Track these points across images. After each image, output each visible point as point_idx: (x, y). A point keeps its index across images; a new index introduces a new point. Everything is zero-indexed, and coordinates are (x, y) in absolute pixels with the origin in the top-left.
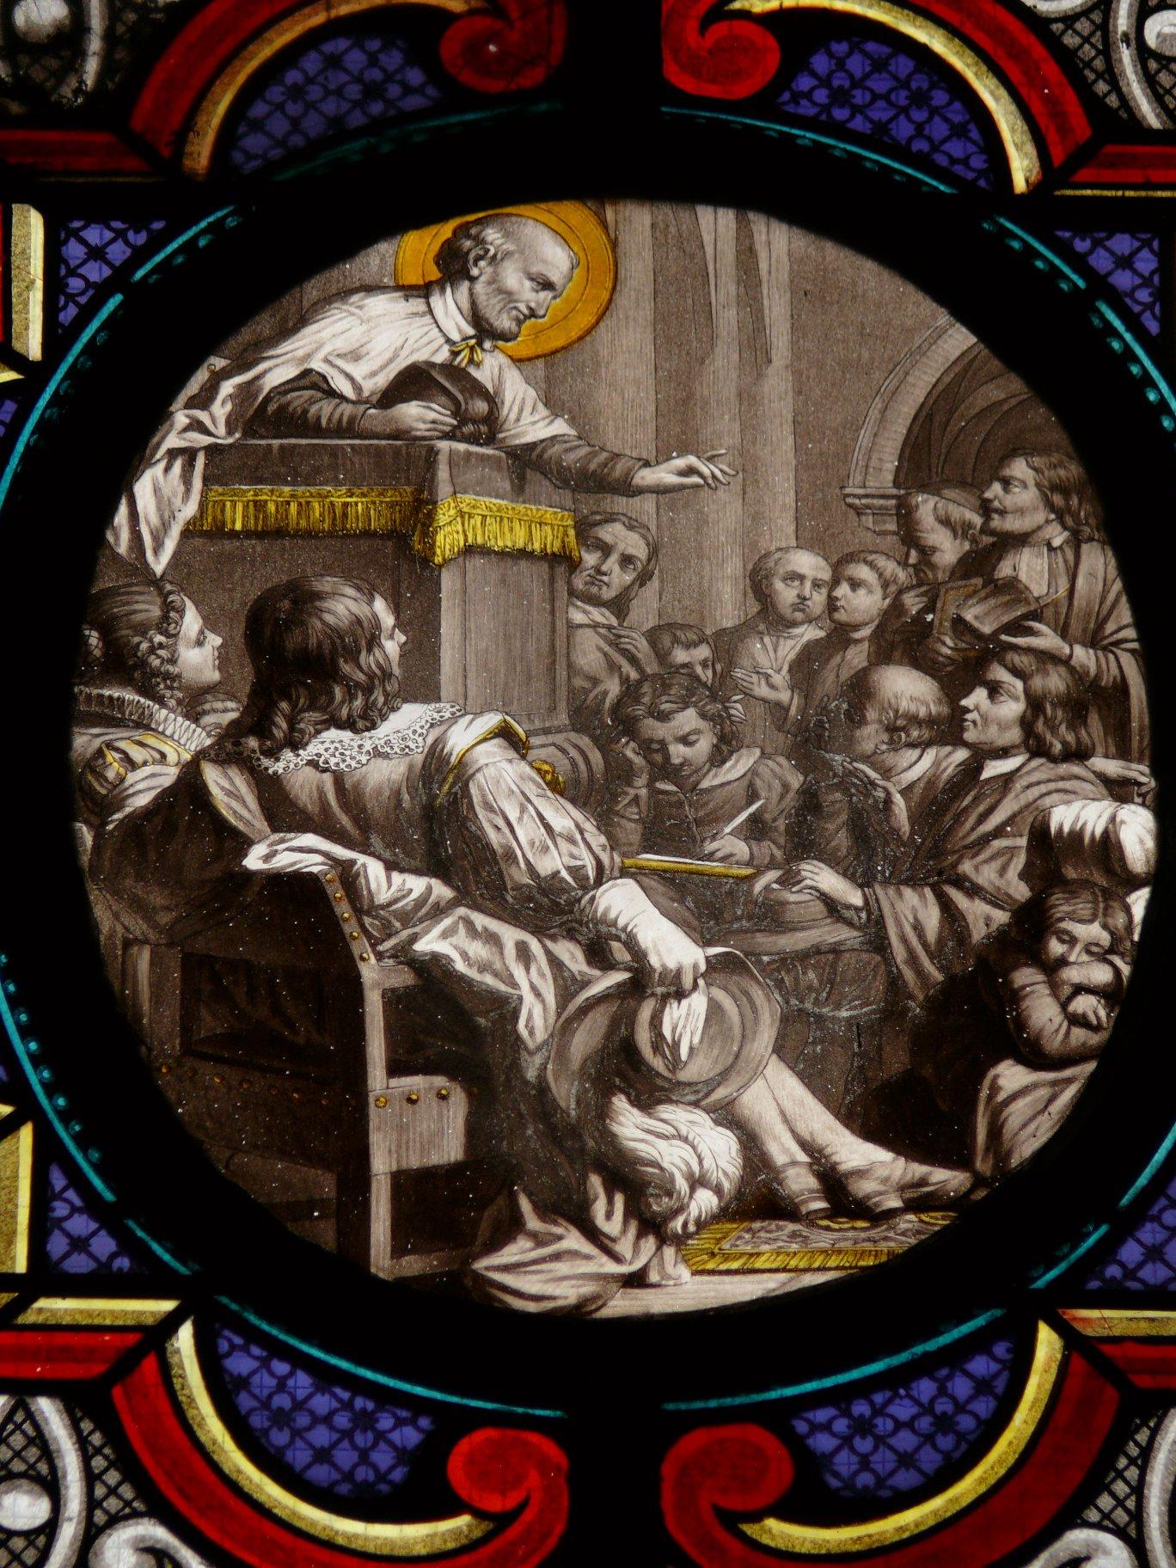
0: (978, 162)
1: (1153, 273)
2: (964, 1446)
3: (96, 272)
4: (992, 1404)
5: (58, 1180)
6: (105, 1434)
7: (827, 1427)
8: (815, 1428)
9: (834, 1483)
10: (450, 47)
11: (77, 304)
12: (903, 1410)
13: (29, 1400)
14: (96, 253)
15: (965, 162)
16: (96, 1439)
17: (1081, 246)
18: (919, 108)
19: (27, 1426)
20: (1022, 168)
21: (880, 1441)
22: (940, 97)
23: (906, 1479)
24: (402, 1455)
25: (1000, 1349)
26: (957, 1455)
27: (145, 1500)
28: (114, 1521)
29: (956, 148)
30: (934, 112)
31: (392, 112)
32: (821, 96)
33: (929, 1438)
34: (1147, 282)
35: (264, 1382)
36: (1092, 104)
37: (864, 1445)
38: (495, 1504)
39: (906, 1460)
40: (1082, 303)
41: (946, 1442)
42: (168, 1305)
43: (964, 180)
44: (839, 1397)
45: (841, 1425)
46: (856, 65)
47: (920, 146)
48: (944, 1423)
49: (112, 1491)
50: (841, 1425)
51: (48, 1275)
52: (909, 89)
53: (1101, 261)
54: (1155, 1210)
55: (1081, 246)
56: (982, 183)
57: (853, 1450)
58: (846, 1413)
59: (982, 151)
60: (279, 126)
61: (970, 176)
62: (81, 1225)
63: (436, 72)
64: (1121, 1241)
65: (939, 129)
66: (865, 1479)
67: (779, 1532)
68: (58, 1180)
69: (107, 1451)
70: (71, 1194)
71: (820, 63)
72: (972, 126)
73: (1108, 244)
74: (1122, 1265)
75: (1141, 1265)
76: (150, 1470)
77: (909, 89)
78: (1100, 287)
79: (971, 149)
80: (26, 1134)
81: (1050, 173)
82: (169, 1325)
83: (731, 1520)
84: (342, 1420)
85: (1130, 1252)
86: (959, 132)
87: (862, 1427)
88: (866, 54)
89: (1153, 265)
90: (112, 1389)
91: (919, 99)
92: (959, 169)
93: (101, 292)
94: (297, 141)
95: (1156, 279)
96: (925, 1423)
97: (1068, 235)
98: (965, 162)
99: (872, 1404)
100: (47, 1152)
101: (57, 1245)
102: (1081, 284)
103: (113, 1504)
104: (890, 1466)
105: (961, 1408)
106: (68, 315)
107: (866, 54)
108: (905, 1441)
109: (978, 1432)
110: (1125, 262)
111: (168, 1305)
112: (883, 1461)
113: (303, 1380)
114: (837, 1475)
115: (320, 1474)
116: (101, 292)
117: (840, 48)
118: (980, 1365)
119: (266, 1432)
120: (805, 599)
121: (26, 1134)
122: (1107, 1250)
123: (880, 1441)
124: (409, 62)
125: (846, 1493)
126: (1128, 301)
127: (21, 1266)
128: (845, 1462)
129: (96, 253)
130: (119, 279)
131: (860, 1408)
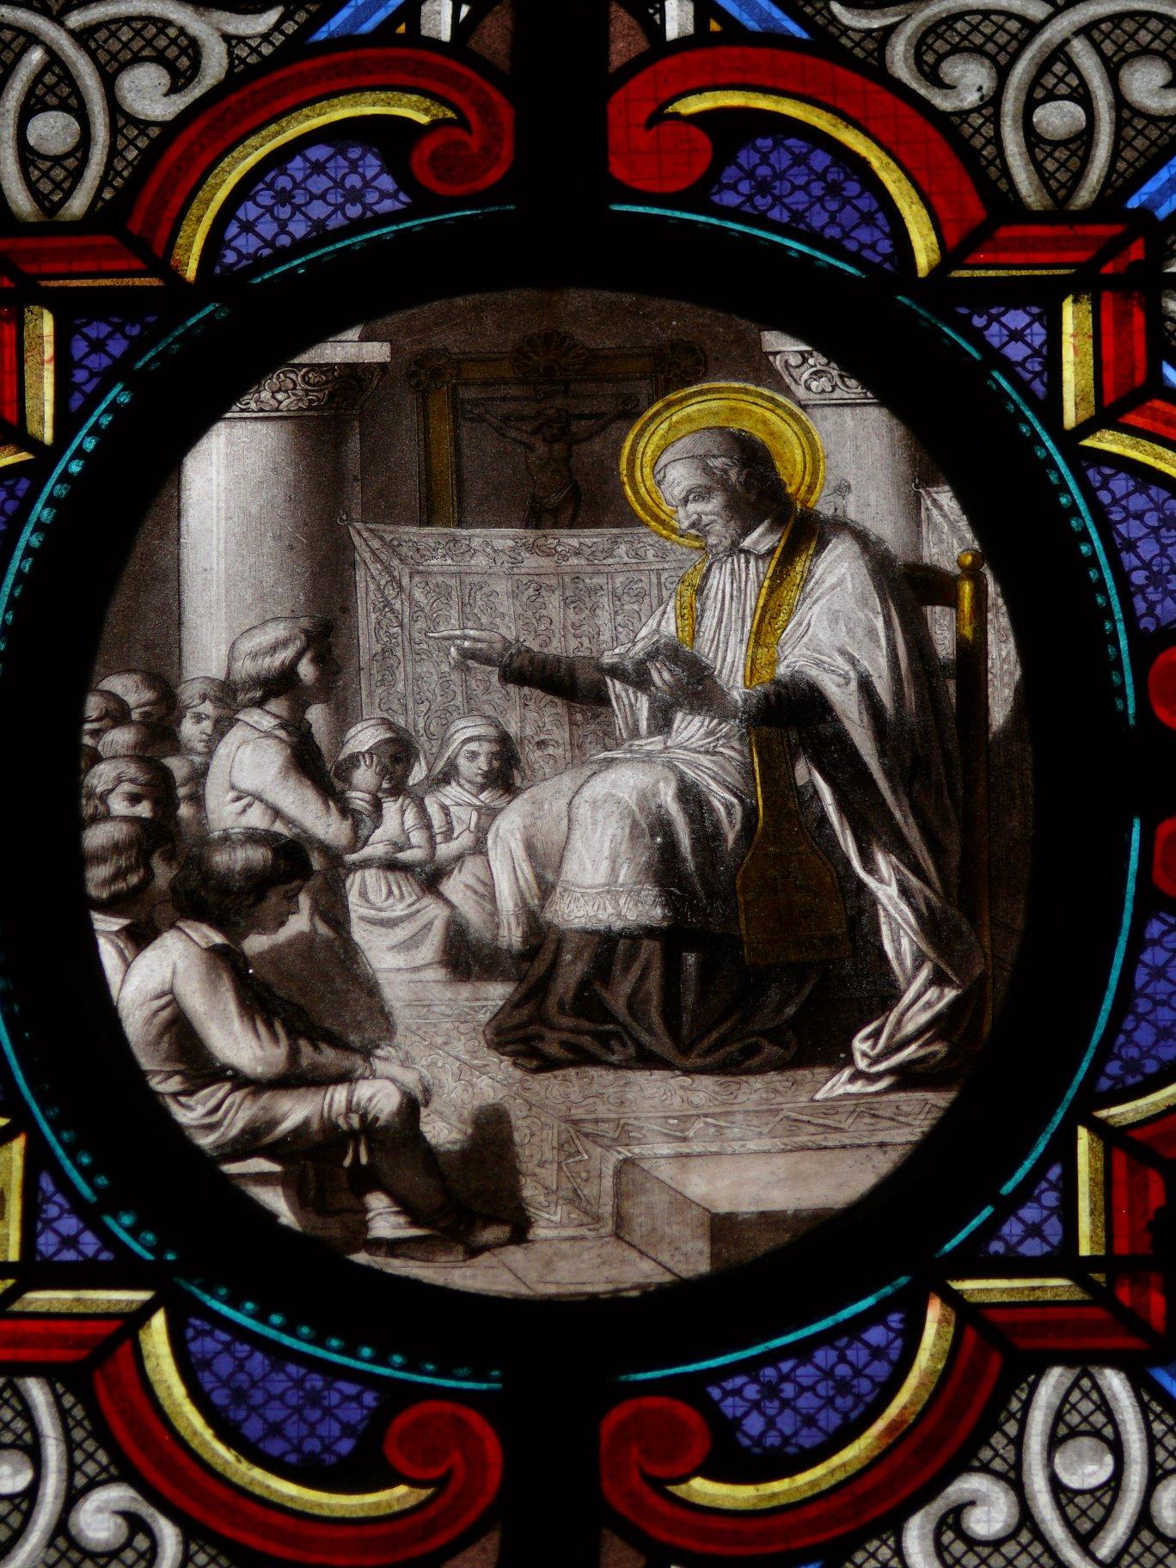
0: (885, 246)
1: (42, 1232)
2: (268, 179)
3: (1030, 1213)
4: (241, 214)
5: (46, 1183)
6: (86, 1408)
7: (384, 195)
8: (394, 196)
9: (746, 1442)
10: (700, 1446)
11: (83, 393)
12: (806, 1374)
13: (19, 1382)
14: (1034, 1230)
15: (873, 247)
16: (78, 1412)
17: (978, 322)
18: (833, 199)
19: (14, 1402)
20: (924, 249)
21: (339, 184)
22: (852, 188)
23: (809, 1439)
24: (347, 1429)
25: (895, 1319)
26: (854, 1415)
27: (118, 1467)
28: (93, 1484)
29: (864, 235)
30: (848, 201)
31: (369, 214)
32: (745, 187)
33: (830, 1401)
34: (48, 1223)
35: (224, 1365)
36: (86, 1397)
37: (354, 181)
38: (436, 1473)
39: (318, 168)
40: (111, 1202)
41: (284, 182)
42: (144, 1296)
43: (872, 263)
44: (749, 1368)
45: (371, 197)
46: (781, 160)
47: (833, 232)
48: (284, 197)
49: (90, 1456)
50: (752, 1391)
51: (34, 1270)
52: (825, 181)
53: (995, 335)
54: (95, 381)
55: (978, 322)
56: (887, 266)
57: (363, 176)
58: (755, 1379)
59: (888, 236)
60: (267, 228)
61: (878, 259)
62: (1016, 352)
63: (405, 181)
64: (1004, 1221)
65: (848, 216)
66: (772, 1440)
67: (703, 1490)
68: (46, 1183)
69: (86, 1423)
70: (59, 1198)
71: (746, 158)
72: (880, 215)
73: (1003, 319)
74: (125, 336)
75: (110, 336)
76: (124, 1438)
77: (825, 181)
78: (996, 358)
79: (878, 234)
80: (18, 1145)
81: (950, 256)
82: (142, 1315)
83: (659, 1485)
84: (293, 1398)
85: (1012, 1229)
86: (867, 219)
87: (355, 196)
88: (788, 149)
89: (41, 1240)
90: (95, 1369)
91: (834, 190)
92: (867, 254)
93: (1025, 1193)
94: (284, 240)
95: (40, 1225)
96: (300, 199)
97: (963, 311)
98: (873, 247)
99: (779, 1371)
100: (37, 1159)
101: (47, 1243)
102: (109, 1220)
103: (91, 1468)
104: (331, 164)
105: (858, 1372)
106: (1055, 1172)
107: (788, 149)
108: (319, 184)
109: (874, 1394)
110: (1016, 336)
111: (144, 1296)
112: (787, 1423)
113: (818, 219)
114: (746, 1434)
115: (275, 1447)
116: (1025, 1193)
117: (765, 143)
118: (876, 1335)
119: (847, 178)
120: (605, 734)
121: (18, 1145)
122: (990, 1229)
123: (339, 184)
124: (737, 1423)
125: (757, 1450)
126: (1019, 369)
127: (1068, 309)
128: (754, 1424)
129: (97, 346)
130: (1008, 1207)
131: (354, 211)
